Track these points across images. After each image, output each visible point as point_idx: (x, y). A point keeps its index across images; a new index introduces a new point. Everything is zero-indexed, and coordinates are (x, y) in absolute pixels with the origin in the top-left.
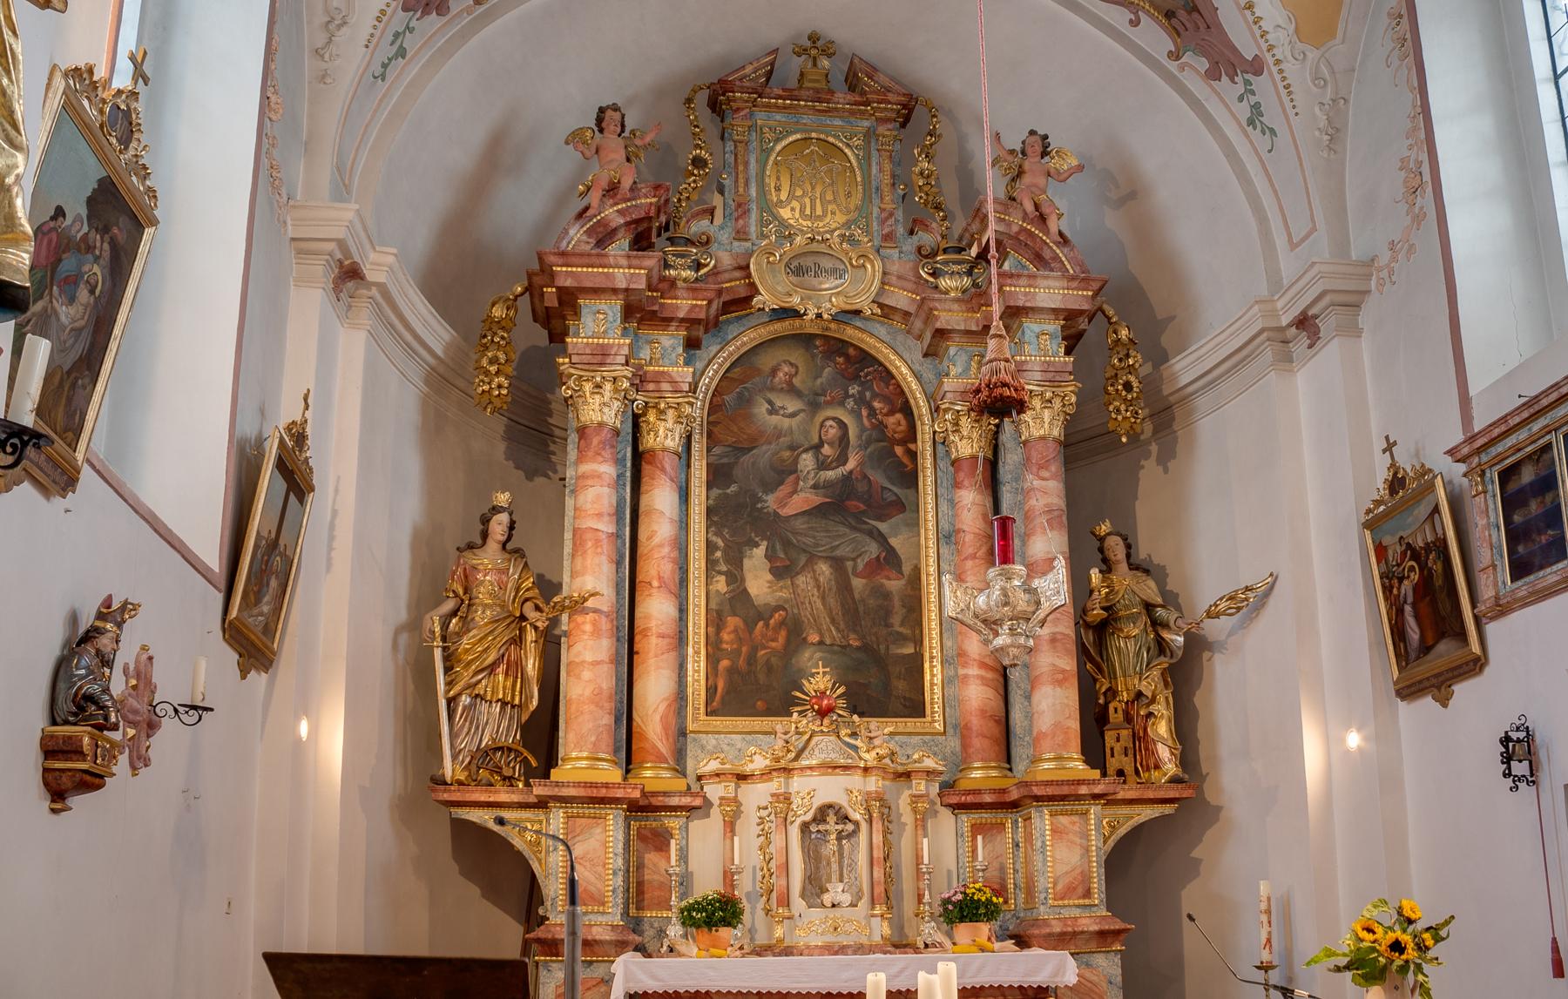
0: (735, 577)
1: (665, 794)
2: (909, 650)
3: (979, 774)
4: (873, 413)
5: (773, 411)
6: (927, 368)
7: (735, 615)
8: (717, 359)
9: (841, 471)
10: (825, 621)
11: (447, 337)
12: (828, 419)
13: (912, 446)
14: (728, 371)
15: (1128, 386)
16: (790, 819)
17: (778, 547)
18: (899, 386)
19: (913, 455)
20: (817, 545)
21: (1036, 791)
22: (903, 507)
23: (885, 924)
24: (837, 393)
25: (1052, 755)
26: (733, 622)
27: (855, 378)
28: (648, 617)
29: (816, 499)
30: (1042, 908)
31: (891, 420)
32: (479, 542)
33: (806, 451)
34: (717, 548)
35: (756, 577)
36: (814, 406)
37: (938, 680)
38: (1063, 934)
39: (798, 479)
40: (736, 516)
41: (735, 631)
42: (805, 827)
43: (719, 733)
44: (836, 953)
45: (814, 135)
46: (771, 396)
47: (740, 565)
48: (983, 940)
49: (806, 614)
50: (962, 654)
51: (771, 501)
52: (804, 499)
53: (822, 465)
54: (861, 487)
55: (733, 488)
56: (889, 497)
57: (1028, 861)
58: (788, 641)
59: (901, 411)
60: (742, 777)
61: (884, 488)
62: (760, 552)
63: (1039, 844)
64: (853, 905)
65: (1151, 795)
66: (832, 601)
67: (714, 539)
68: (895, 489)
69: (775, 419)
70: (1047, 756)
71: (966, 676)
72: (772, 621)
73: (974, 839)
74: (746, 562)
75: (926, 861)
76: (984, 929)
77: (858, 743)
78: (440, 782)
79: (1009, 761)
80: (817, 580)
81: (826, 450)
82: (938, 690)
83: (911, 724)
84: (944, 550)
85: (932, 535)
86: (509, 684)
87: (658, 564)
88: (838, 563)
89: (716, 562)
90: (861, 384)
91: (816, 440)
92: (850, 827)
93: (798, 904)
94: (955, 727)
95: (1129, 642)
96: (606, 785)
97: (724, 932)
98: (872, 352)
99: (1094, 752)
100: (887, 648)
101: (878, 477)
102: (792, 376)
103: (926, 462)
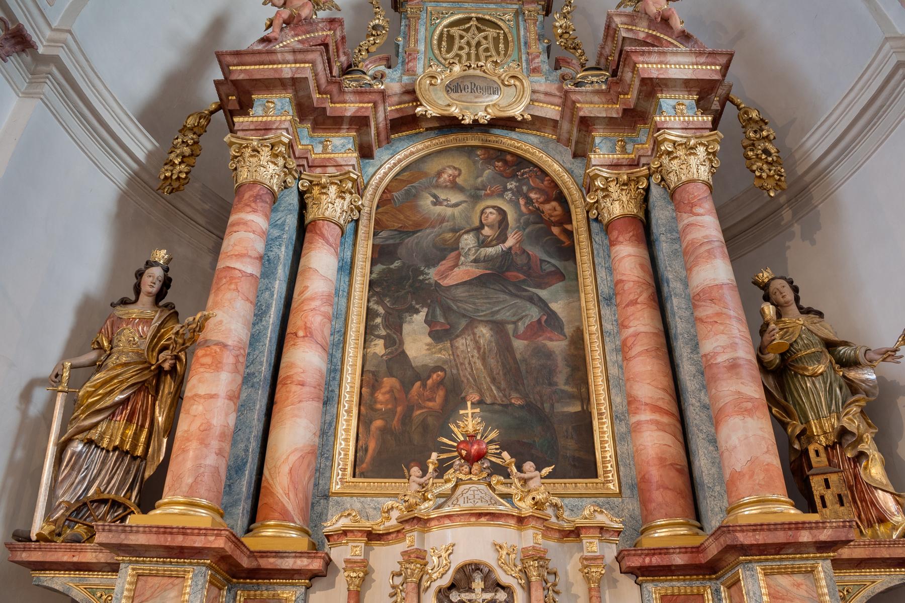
0: (394, 341)
1: (277, 554)
2: (575, 408)
3: (667, 532)
4: (529, 201)
5: (437, 202)
6: (577, 166)
7: (391, 375)
8: (388, 164)
9: (499, 248)
10: (486, 381)
11: (149, 146)
12: (488, 207)
13: (568, 227)
14: (398, 174)
15: (766, 152)
16: (425, 584)
17: (438, 312)
18: (553, 181)
19: (570, 234)
20: (478, 311)
21: (745, 539)
22: (567, 277)
24: (497, 187)
25: (753, 498)
26: (389, 382)
27: (513, 176)
28: (291, 365)
29: (477, 271)
31: (547, 207)
32: (133, 298)
33: (467, 232)
34: (377, 315)
35: (414, 341)
36: (475, 196)
39: (460, 255)
40: (398, 284)
41: (391, 391)
43: (364, 495)
45: (473, 15)
46: (437, 192)
47: (399, 330)
49: (465, 374)
50: (631, 401)
51: (432, 274)
52: (465, 271)
53: (483, 243)
54: (520, 261)
55: (397, 264)
56: (548, 268)
58: (446, 400)
59: (556, 200)
60: (372, 537)
61: (542, 261)
62: (420, 318)
65: (885, 553)
66: (492, 362)
67: (376, 307)
68: (553, 261)
69: (438, 209)
70: (747, 499)
71: (639, 423)
72: (430, 382)
74: (406, 328)
77: (513, 490)
78: (22, 537)
79: (698, 517)
80: (477, 342)
81: (487, 231)
82: (609, 447)
83: (582, 485)
84: (606, 311)
85: (592, 296)
86: (130, 432)
87: (313, 312)
88: (498, 327)
89: (376, 327)
90: (519, 181)
91: (477, 223)
94: (632, 487)
95: (816, 379)
96: (183, 531)
98: (528, 156)
99: (803, 496)
100: (552, 406)
101: (536, 252)
102: (455, 177)
103: (582, 237)
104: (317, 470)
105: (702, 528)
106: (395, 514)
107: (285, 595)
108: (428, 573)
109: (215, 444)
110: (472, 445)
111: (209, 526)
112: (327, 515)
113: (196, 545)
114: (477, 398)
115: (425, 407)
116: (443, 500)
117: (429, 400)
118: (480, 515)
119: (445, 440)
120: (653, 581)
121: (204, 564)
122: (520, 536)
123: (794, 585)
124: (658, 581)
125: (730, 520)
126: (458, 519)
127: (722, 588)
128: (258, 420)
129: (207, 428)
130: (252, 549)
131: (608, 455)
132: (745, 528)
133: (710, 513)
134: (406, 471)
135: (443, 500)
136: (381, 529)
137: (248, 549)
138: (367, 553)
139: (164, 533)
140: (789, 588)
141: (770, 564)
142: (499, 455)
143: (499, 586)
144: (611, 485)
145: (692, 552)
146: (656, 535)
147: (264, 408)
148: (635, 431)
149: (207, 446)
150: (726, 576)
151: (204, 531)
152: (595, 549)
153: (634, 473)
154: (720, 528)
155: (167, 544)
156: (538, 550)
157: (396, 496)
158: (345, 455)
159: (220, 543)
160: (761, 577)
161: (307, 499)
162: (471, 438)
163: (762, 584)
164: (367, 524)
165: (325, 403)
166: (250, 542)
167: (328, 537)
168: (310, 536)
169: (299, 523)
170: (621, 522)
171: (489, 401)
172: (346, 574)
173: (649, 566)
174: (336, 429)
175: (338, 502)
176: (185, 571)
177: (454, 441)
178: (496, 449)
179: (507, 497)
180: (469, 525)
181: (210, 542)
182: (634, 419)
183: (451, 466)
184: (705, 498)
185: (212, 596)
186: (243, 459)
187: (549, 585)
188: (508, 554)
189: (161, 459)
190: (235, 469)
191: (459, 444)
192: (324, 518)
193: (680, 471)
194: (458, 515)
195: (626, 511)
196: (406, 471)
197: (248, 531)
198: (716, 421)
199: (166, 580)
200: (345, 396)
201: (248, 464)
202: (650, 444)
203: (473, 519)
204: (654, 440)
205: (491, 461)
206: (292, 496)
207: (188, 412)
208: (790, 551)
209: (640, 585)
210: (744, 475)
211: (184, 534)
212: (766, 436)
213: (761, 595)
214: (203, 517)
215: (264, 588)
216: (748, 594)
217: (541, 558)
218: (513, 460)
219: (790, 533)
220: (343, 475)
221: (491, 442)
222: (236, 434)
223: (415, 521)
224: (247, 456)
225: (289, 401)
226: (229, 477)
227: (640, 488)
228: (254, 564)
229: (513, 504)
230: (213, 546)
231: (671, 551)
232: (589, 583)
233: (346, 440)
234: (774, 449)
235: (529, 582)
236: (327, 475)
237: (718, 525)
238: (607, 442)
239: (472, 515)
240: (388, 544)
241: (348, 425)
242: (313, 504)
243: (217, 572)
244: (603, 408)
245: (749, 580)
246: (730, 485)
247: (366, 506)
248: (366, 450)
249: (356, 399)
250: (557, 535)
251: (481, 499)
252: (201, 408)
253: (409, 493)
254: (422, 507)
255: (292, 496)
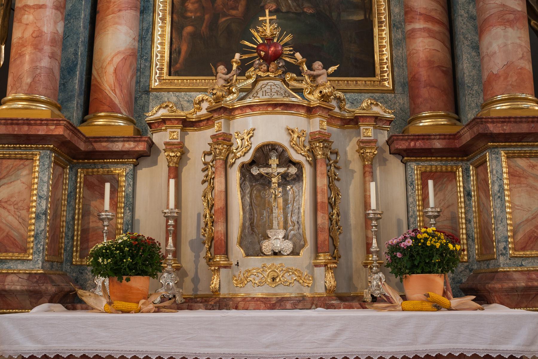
1: (109, 139)
2: (359, 17)
16: (230, 161)
21: (493, 128)
23: (330, 275)
25: (505, 96)
30: (502, 259)
37: (387, 56)
38: (528, 289)
42: (245, 169)
43: (179, 90)
44: (272, 307)
48: (437, 295)
57: (483, 209)
58: (247, 8)
60: (187, 124)
63: (496, 188)
64: (295, 252)
70: (499, 97)
71: (413, 30)
73: (425, 186)
75: (373, 206)
76: (438, 281)
77: (303, 85)
83: (362, 82)
92: (293, 170)
93: (237, 252)
94: (403, 85)
96: (28, 122)
97: (138, 283)
104: (138, 70)
105: (459, 120)
106: (205, 105)
107: (117, 172)
108: (233, 152)
109: (47, 49)
110: (270, 48)
111: (49, 117)
112: (148, 107)
113: (40, 133)
114: (274, 7)
115: (229, 15)
116: (244, 94)
117: (233, 9)
118: (275, 105)
119: (247, 43)
120: (416, 161)
121: (48, 149)
122: (309, 123)
123: (530, 166)
124: (420, 161)
125: (484, 113)
126: (258, 109)
127: (471, 168)
128: (84, 27)
129: (39, 36)
130: (87, 135)
131: (385, 58)
132: (495, 120)
133: (467, 108)
134: (213, 69)
135: (244, 94)
136: (193, 118)
137: (84, 136)
138: (183, 137)
139: (12, 124)
140: (525, 168)
141: (513, 149)
142: (292, 56)
143: (291, 162)
144: (386, 83)
145: (449, 139)
146: (421, 124)
147: (88, 17)
148: (409, 38)
149: (41, 50)
150: (476, 158)
151: (45, 122)
152: (370, 134)
153: (406, 73)
154: (474, 119)
155: (15, 133)
156: (324, 134)
157: (205, 91)
158: (162, 57)
159: (59, 131)
160: (503, 159)
161: (130, 94)
162: (268, 41)
163: (504, 164)
164: (182, 114)
165: (142, 12)
166: (84, 129)
167: (150, 125)
168: (135, 124)
169: (125, 114)
170: (393, 113)
171: (284, 9)
172: (166, 154)
173: (413, 149)
174: (152, 34)
175: (157, 97)
176: (33, 154)
177: (254, 43)
178: (290, 51)
179: (299, 91)
180: (267, 113)
181: (52, 130)
182: (409, 27)
183: (251, 65)
184: (464, 95)
185: (57, 173)
186: (73, 62)
187: (331, 162)
188: (299, 137)
189: (2, 63)
190: (67, 70)
191: (259, 46)
192: (146, 110)
193: (445, 73)
194: (258, 105)
195: (398, 104)
196: (213, 69)
197: (83, 121)
198: (480, 30)
199: (17, 162)
200: (159, 6)
201: (78, 66)
202: (421, 49)
203: (270, 109)
204: (424, 46)
205: (285, 61)
206: (117, 91)
207: (20, 21)
208: (531, 139)
209: (405, 163)
210: (500, 77)
211: (29, 124)
212: (523, 44)
213: (502, 173)
214: (43, 110)
215: (99, 166)
216: (491, 172)
217: (325, 141)
218: (304, 59)
219: (533, 125)
220: (160, 74)
221: (286, 45)
222: (65, 40)
223: (222, 111)
224: (77, 59)
225: (110, 10)
226: (63, 77)
227: (409, 85)
228: (90, 148)
229: (303, 97)
230: (54, 133)
231: (433, 137)
232: (364, 161)
233: (162, 44)
234: (529, 56)
235: (315, 159)
236: (147, 74)
237: (473, 117)
238: (385, 46)
239: (269, 105)
240: (200, 130)
241: (163, 31)
242: (136, 98)
243: (59, 154)
244: (383, 17)
245: (494, 161)
246: (486, 85)
247: (181, 99)
248: (179, 52)
249: (168, 8)
250: (339, 123)
251: (277, 92)
252: (31, 17)
253: (216, 87)
254: (228, 99)
255: (117, 91)
